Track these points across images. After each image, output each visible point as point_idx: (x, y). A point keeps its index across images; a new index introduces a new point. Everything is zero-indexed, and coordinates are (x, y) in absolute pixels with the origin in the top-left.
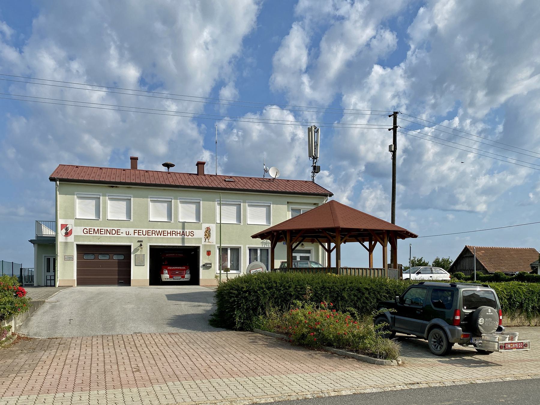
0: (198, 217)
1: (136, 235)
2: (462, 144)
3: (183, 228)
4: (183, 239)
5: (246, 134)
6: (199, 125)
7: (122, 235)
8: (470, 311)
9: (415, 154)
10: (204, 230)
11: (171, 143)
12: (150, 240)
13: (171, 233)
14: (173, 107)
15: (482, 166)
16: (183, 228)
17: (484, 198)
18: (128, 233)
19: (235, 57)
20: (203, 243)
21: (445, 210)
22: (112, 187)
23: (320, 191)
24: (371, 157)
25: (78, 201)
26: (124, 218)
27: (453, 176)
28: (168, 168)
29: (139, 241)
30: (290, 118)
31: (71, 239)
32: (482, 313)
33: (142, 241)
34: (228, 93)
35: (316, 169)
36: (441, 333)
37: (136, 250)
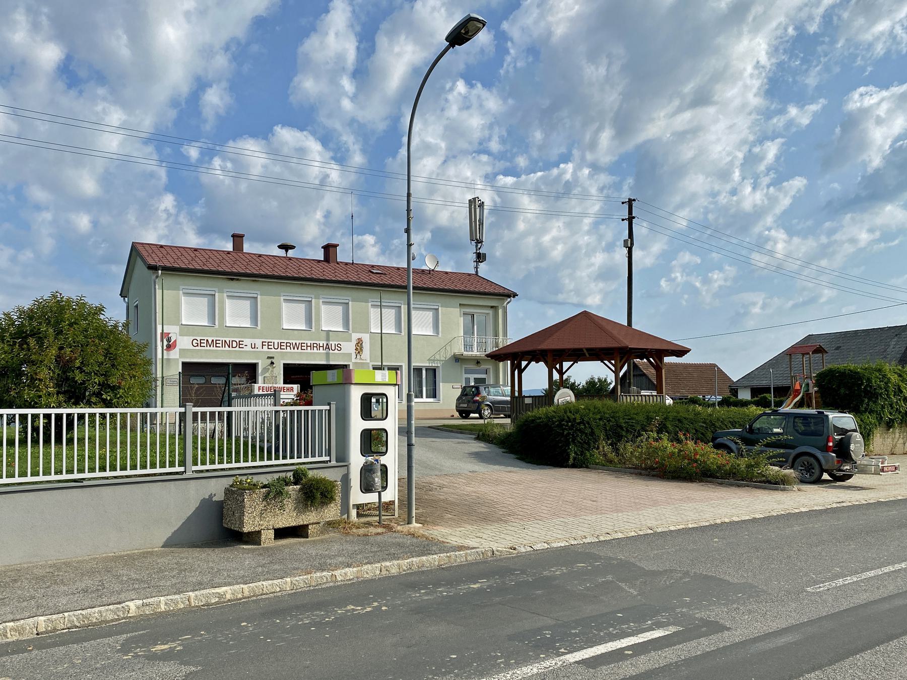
0: (346, 323)
1: (265, 348)
2: (573, 205)
3: (328, 339)
4: (328, 355)
5: (240, 169)
6: (159, 150)
7: (246, 349)
8: (840, 437)
9: (506, 212)
10: (354, 342)
11: (106, 180)
12: (283, 355)
13: (312, 347)
14: (116, 116)
15: (601, 237)
16: (328, 339)
17: (601, 285)
18: (254, 347)
19: (234, 40)
20: (354, 360)
21: (543, 302)
22: (232, 279)
23: (501, 291)
24: (443, 218)
25: (183, 299)
26: (247, 324)
27: (558, 252)
28: (287, 251)
29: (268, 358)
30: (314, 146)
31: (174, 354)
32: (852, 441)
33: (273, 358)
34: (214, 98)
35: (480, 258)
36: (812, 460)
37: (265, 370)
